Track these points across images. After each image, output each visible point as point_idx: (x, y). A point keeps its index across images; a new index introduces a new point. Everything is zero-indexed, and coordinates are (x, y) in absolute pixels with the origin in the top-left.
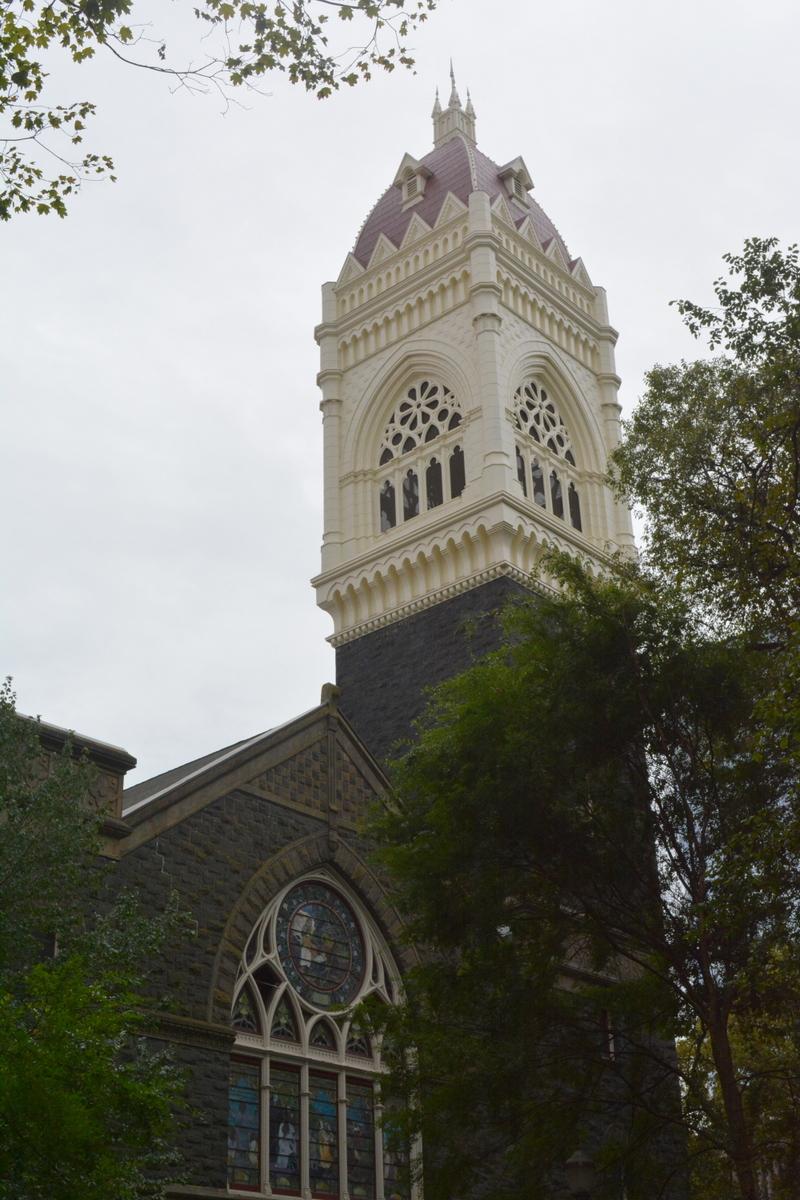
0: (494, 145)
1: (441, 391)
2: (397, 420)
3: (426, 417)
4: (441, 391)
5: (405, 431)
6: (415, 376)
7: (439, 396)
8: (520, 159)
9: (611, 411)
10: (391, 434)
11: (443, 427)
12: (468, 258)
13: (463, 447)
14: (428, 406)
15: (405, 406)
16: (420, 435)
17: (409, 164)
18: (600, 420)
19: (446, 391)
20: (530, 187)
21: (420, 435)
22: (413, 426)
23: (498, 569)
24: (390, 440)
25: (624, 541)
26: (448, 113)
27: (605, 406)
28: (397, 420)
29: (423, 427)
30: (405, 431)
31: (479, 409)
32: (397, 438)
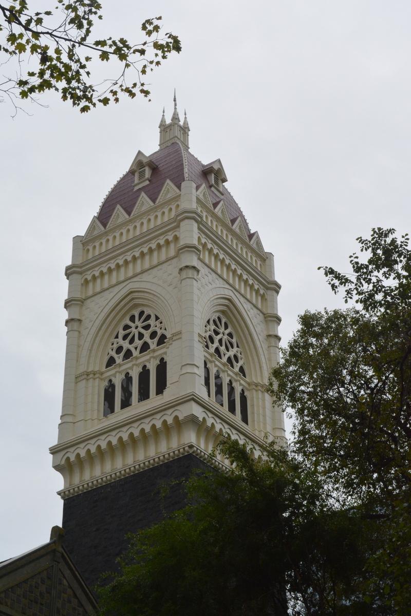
0: (201, 150)
1: (153, 317)
2: (120, 336)
3: (141, 336)
4: (153, 317)
5: (126, 345)
6: (136, 306)
7: (152, 322)
8: (219, 161)
9: (273, 340)
10: (115, 346)
11: (153, 344)
12: (178, 226)
13: (166, 359)
14: (143, 328)
15: (127, 327)
16: (136, 348)
17: (140, 158)
18: (265, 346)
19: (157, 318)
20: (224, 180)
21: (136, 348)
22: (131, 342)
23: (187, 448)
24: (115, 350)
25: (278, 434)
26: (170, 125)
27: (269, 336)
28: (120, 336)
29: (138, 343)
30: (126, 345)
31: (180, 333)
32: (119, 350)
